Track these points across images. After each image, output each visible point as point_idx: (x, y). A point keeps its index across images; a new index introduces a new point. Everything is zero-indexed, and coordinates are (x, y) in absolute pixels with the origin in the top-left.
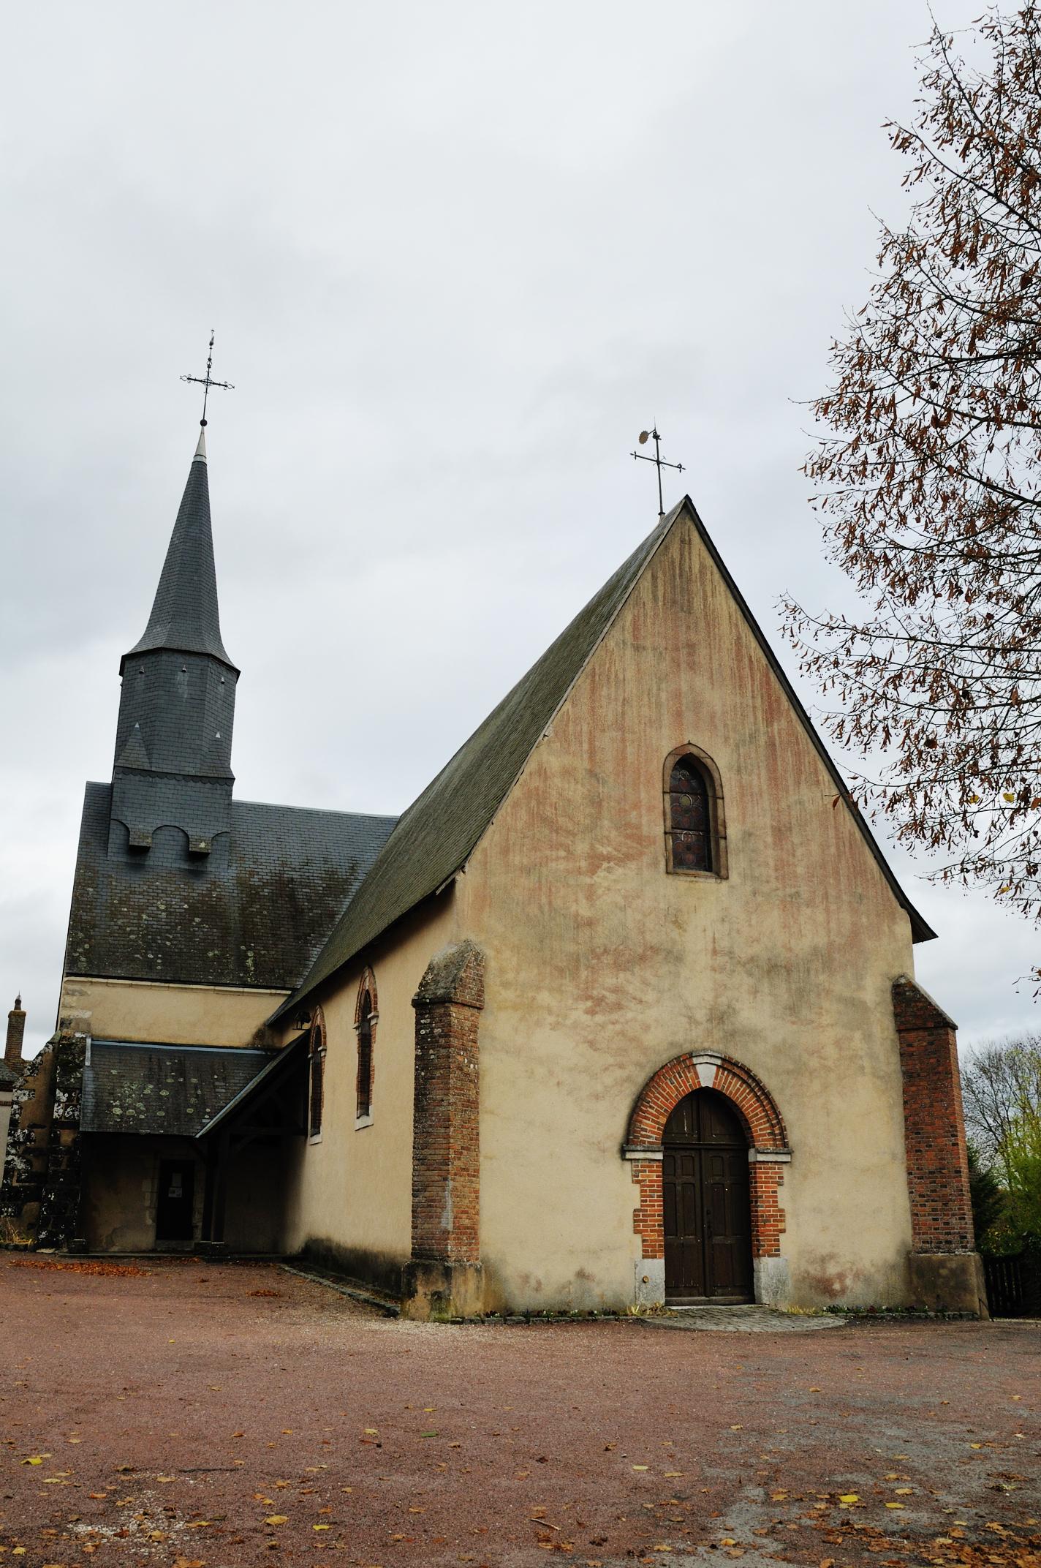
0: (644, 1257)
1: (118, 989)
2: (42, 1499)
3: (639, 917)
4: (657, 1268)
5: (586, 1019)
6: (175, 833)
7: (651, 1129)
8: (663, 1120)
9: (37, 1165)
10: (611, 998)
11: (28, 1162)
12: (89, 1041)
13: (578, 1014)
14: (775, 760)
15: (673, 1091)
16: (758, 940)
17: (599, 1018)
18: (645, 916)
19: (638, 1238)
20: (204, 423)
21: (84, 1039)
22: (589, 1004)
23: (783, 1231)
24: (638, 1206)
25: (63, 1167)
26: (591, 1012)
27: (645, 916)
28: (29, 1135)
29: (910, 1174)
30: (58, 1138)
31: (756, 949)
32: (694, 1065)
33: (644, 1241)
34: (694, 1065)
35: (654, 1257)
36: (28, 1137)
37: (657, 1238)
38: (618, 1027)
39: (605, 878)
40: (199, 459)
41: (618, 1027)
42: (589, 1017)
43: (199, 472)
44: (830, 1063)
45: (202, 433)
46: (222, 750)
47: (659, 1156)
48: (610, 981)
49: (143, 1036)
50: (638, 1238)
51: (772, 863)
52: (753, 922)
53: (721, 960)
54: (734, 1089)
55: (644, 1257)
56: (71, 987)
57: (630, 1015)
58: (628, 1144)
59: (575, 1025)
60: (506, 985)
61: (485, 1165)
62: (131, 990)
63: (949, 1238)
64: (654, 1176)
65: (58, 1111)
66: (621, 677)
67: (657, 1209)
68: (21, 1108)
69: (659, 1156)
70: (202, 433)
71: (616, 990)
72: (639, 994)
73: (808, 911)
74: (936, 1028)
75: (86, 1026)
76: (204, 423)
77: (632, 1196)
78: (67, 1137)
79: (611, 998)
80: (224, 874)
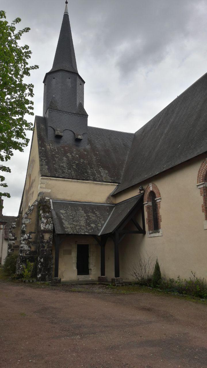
1: (60, 182)
2: (14, 102)
6: (70, 132)
9: (33, 249)
11: (30, 247)
12: (51, 200)
14: (87, 284)
21: (49, 199)
25: (46, 248)
28: (29, 236)
30: (43, 237)
36: (29, 238)
40: (66, 13)
43: (66, 18)
45: (66, 6)
46: (81, 106)
49: (69, 198)
56: (43, 181)
62: (65, 182)
65: (42, 227)
68: (26, 226)
70: (66, 6)
75: (49, 195)
78: (47, 236)
80: (85, 146)
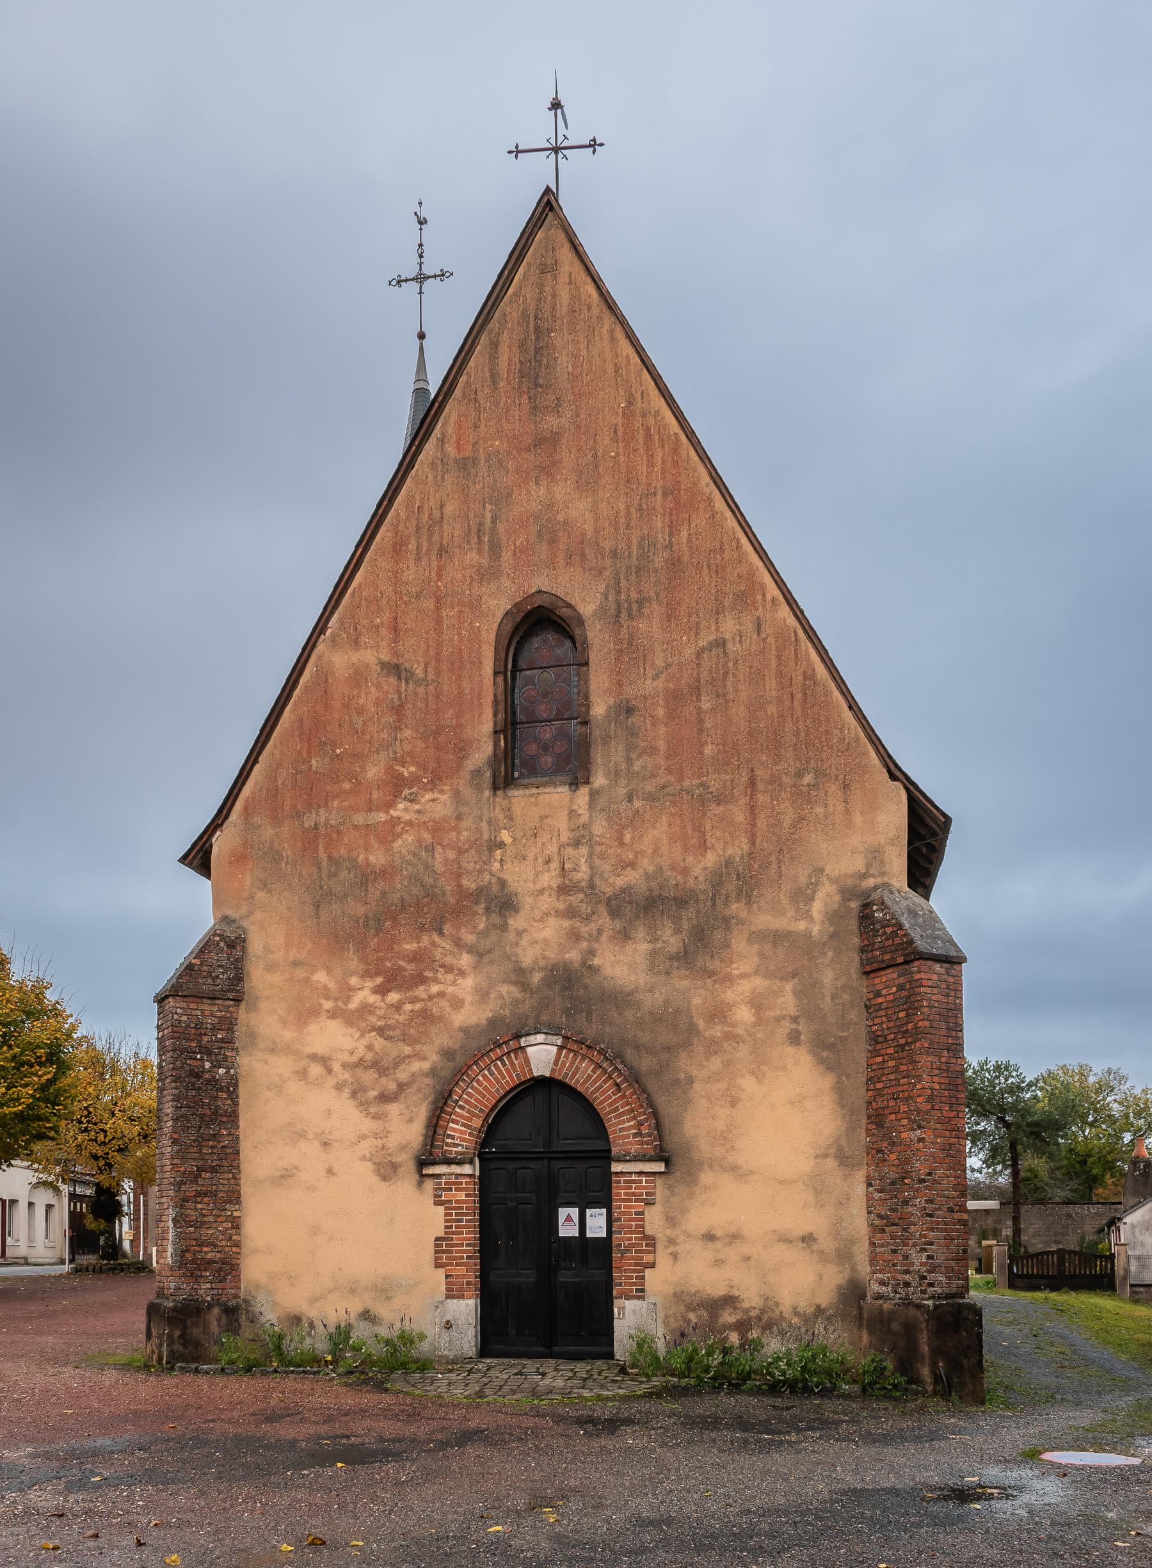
0: (448, 1297)
3: (451, 855)
4: (466, 1309)
5: (373, 999)
7: (461, 1134)
8: (477, 1123)
10: (410, 968)
13: (364, 994)
15: (486, 1088)
16: (632, 865)
17: (393, 997)
18: (460, 852)
19: (441, 1273)
20: (422, 336)
22: (379, 980)
23: (653, 1265)
24: (441, 1234)
26: (381, 990)
27: (460, 852)
29: (869, 1185)
31: (631, 878)
32: (522, 1048)
33: (447, 1277)
34: (522, 1048)
35: (462, 1297)
37: (468, 1273)
38: (418, 1006)
39: (406, 810)
40: (421, 385)
41: (418, 1006)
42: (379, 997)
44: (740, 1031)
45: (421, 349)
47: (616, 1167)
48: (410, 947)
50: (441, 1273)
51: (662, 745)
52: (627, 838)
53: (576, 899)
54: (583, 1075)
55: (448, 1297)
57: (435, 989)
58: (427, 1159)
59: (366, 1009)
60: (271, 968)
61: (246, 1189)
63: (907, 1277)
64: (464, 1196)
66: (437, 514)
67: (467, 1238)
69: (616, 1167)
70: (421, 349)
71: (415, 958)
72: (448, 960)
73: (719, 810)
74: (906, 962)
76: (422, 336)
77: (435, 1220)
79: (410, 968)
